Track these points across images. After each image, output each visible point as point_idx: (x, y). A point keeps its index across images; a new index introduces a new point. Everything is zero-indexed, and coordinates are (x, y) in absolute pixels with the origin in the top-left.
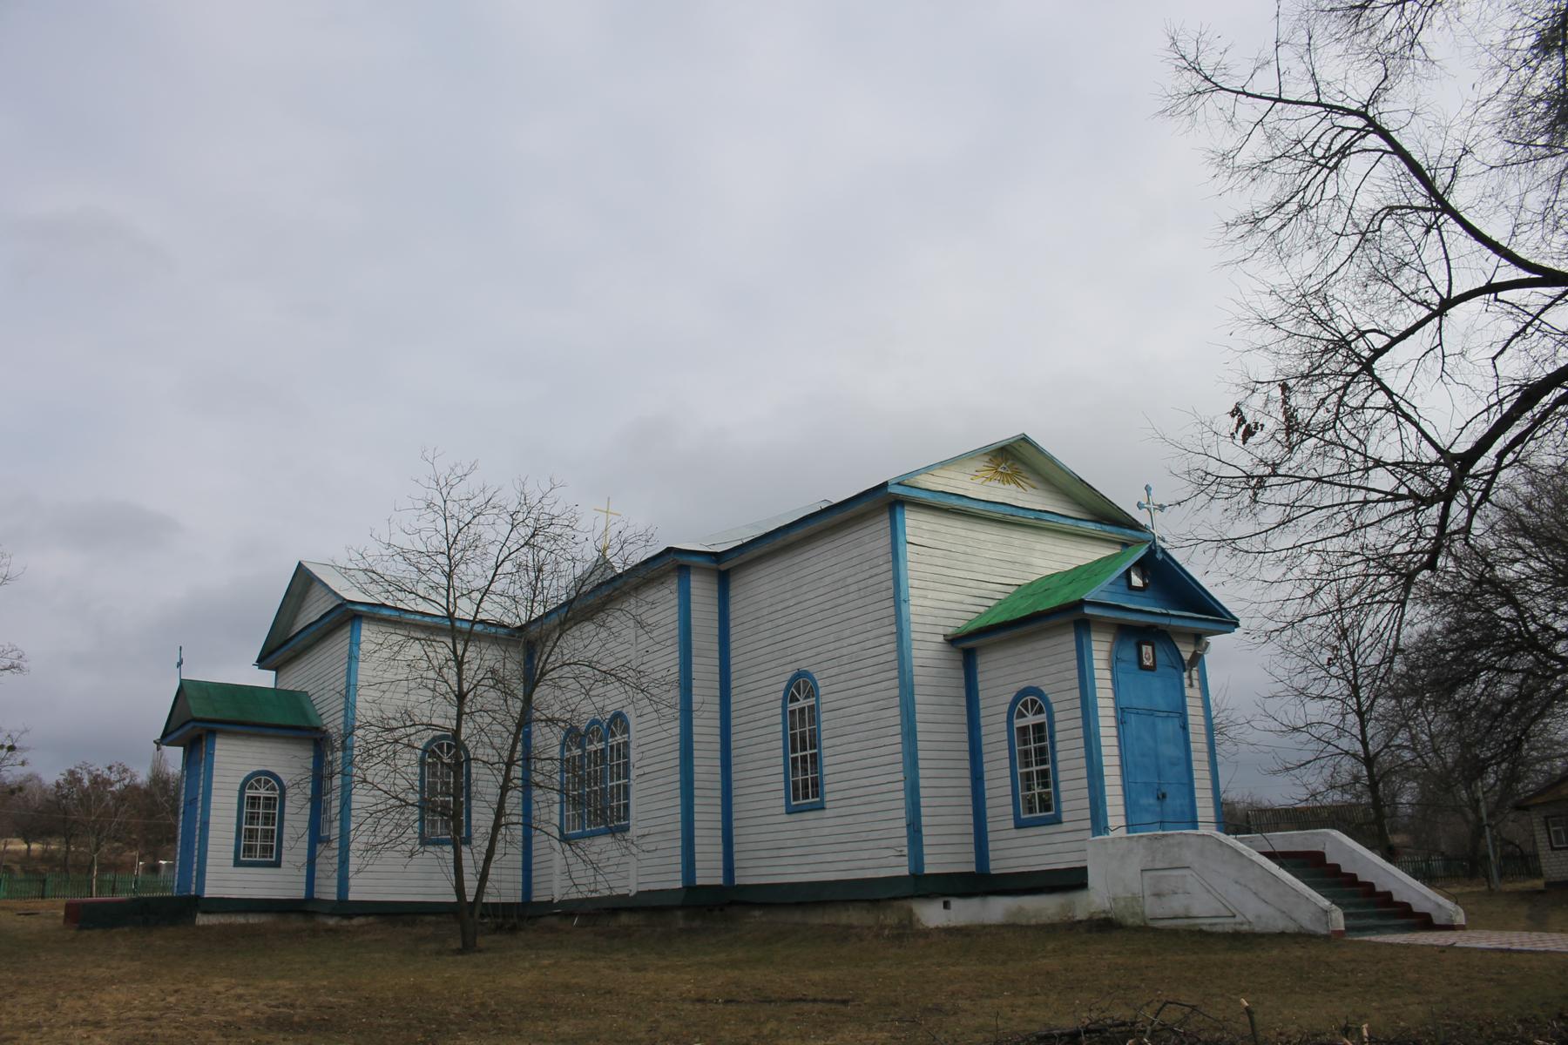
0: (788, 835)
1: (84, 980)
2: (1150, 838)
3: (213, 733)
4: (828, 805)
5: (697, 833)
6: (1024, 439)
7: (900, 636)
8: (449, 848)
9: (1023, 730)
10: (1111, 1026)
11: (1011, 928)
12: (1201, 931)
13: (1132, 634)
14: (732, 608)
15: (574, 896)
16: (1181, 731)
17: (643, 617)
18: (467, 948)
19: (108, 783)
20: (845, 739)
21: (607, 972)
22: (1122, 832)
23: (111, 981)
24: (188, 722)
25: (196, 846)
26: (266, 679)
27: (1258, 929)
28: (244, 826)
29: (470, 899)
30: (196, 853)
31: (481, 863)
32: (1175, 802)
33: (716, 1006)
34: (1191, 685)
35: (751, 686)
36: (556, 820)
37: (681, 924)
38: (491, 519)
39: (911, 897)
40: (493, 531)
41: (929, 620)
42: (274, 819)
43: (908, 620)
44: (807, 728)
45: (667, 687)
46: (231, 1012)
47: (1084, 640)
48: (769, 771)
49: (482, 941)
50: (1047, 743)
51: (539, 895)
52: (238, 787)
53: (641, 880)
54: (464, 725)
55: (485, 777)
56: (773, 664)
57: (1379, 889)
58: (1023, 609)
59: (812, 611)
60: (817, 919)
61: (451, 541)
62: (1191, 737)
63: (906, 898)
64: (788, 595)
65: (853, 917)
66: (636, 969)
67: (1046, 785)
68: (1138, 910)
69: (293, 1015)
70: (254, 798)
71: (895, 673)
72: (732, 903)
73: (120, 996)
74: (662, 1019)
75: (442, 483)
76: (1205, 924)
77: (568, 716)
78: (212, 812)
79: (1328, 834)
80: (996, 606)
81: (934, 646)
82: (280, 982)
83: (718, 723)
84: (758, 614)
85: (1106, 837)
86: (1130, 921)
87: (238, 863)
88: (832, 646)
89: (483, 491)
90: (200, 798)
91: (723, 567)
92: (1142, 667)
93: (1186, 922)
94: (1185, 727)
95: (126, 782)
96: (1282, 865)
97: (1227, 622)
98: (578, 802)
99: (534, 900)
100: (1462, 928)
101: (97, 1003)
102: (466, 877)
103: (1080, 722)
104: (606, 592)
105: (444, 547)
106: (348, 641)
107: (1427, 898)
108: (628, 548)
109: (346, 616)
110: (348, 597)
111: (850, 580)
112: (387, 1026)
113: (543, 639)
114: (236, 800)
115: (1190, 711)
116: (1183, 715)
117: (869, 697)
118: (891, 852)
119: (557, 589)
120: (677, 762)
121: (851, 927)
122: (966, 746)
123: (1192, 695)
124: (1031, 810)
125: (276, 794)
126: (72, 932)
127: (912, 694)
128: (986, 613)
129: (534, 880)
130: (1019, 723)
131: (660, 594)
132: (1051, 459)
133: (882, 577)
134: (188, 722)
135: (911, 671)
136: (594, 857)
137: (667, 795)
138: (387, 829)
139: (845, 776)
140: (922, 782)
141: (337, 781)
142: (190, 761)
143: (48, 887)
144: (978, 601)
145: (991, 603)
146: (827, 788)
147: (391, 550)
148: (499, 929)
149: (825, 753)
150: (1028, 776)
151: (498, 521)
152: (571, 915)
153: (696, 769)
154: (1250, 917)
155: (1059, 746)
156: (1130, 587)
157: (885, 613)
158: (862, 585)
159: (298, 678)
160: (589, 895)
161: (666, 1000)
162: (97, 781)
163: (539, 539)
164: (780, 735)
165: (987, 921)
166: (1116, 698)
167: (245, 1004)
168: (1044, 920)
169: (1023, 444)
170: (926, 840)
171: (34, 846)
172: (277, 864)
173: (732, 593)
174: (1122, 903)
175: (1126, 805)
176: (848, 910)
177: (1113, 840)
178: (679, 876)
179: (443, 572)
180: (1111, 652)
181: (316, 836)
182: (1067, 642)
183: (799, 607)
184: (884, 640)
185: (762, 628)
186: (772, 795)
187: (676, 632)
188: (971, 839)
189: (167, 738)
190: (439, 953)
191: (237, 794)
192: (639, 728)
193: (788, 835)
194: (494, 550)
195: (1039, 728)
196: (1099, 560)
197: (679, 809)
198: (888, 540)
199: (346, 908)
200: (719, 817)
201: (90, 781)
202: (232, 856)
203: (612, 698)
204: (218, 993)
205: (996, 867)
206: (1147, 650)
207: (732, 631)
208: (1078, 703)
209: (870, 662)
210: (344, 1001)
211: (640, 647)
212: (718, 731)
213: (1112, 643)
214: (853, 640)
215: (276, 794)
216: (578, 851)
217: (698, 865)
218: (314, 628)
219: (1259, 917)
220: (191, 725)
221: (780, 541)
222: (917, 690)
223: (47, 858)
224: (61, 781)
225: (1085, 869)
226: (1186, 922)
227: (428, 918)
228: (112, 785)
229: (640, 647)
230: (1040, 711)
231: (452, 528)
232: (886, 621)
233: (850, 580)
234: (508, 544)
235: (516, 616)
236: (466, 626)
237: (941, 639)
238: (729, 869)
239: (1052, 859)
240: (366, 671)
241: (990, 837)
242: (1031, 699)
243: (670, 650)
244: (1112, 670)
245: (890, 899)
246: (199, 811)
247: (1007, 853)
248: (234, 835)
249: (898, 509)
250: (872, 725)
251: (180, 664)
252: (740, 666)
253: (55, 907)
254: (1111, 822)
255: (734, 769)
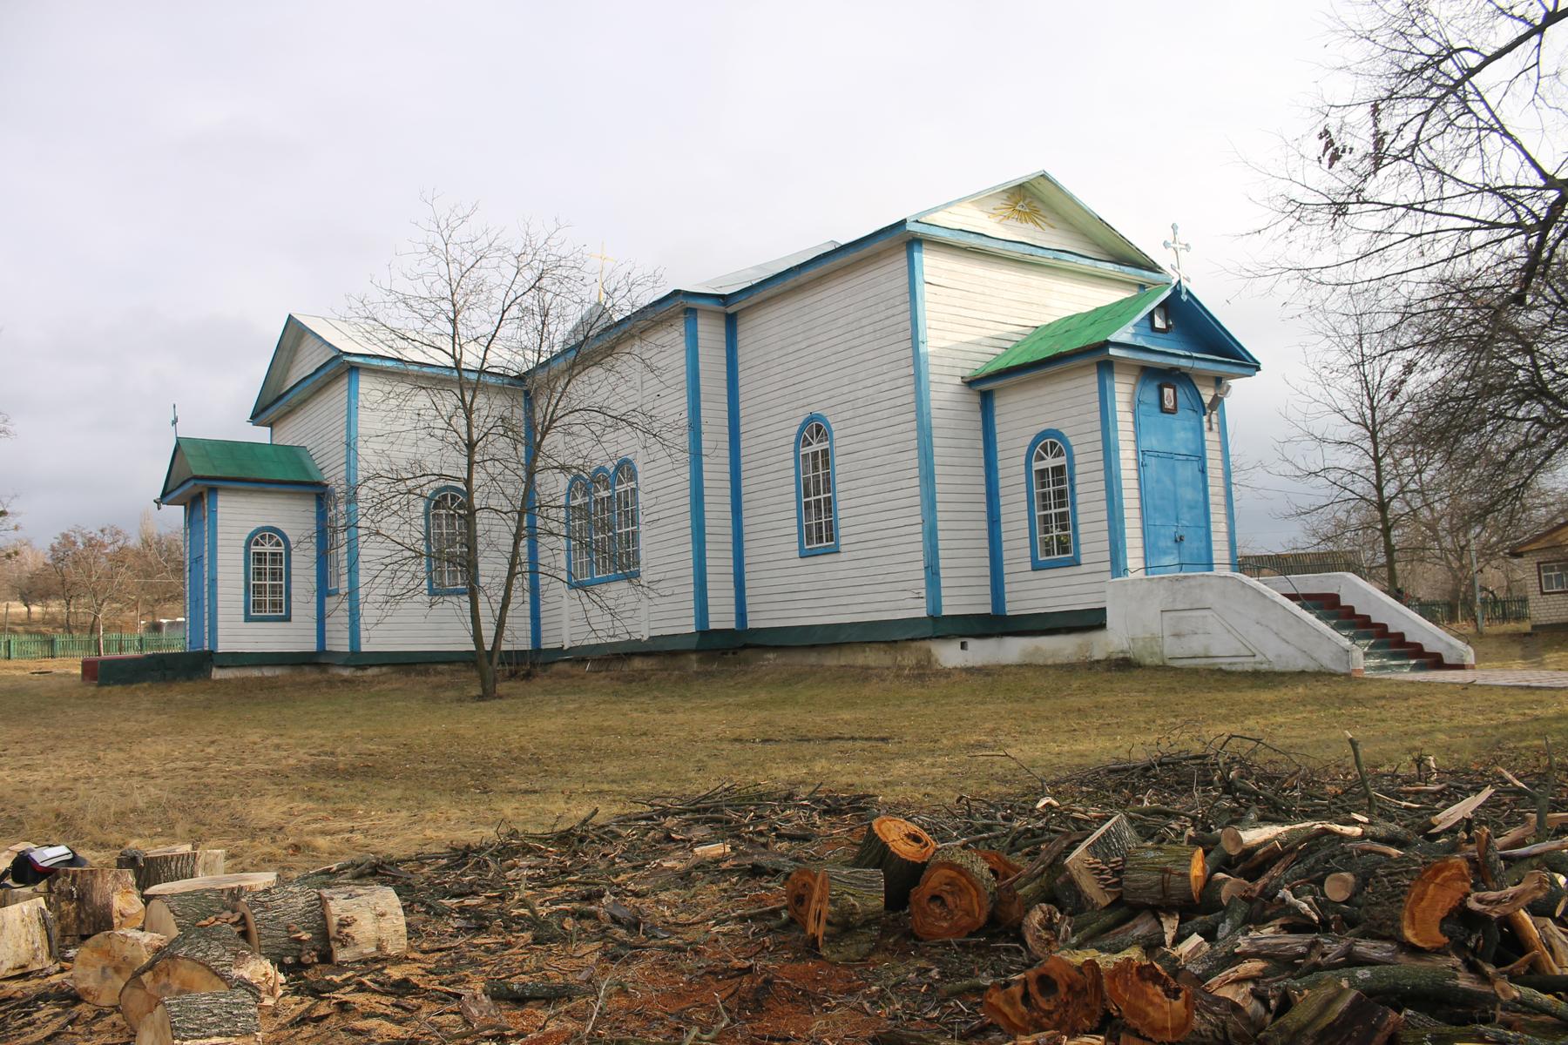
0: (801, 579)
1: (117, 733)
2: (1171, 580)
3: (214, 491)
4: (842, 549)
5: (709, 578)
6: (1044, 176)
7: (917, 377)
8: (466, 598)
9: (1042, 473)
10: (1185, 759)
11: (1025, 668)
12: (1220, 670)
13: (1159, 377)
14: (740, 352)
15: (593, 642)
16: (1199, 474)
17: (653, 360)
18: (487, 695)
19: (102, 545)
20: (859, 483)
21: (635, 715)
22: (1141, 574)
23: (144, 734)
24: (188, 480)
25: (206, 602)
26: (261, 435)
27: (1277, 668)
28: (252, 582)
29: (488, 648)
30: (206, 609)
31: (498, 613)
32: (1193, 545)
33: (754, 746)
34: (1211, 429)
35: (762, 431)
36: (564, 566)
37: (695, 667)
38: (495, 262)
39: (930, 638)
40: (499, 277)
41: (947, 362)
42: (281, 575)
43: (926, 362)
44: (821, 472)
45: (680, 431)
46: (277, 761)
47: (1107, 382)
48: (783, 516)
49: (502, 688)
50: (1067, 486)
51: (548, 642)
52: (243, 544)
53: (653, 625)
54: (475, 476)
55: (497, 528)
56: (785, 408)
57: (1391, 630)
58: (1045, 351)
59: (824, 353)
60: (832, 660)
61: (454, 287)
62: (1209, 480)
63: (924, 639)
64: (799, 338)
65: (870, 658)
66: (663, 711)
67: (1064, 528)
68: (1157, 649)
69: (337, 763)
70: (259, 554)
71: (912, 416)
72: (746, 647)
73: (159, 748)
74: (705, 759)
75: (443, 226)
76: (1224, 663)
77: (581, 461)
78: (219, 569)
79: (1344, 577)
80: (1013, 348)
81: (952, 389)
82: (314, 732)
83: (728, 468)
84: (768, 358)
85: (1125, 578)
86: (1148, 661)
87: (248, 618)
88: (846, 389)
89: (486, 232)
90: (206, 555)
91: (730, 310)
92: (1163, 409)
93: (1204, 661)
94: (1203, 471)
95: (120, 544)
96: (1303, 606)
97: (1249, 364)
98: (587, 547)
99: (543, 647)
100: (1472, 667)
101: (138, 755)
102: (483, 626)
103: (1101, 465)
104: (613, 335)
105: (447, 293)
106: (346, 393)
107: (1439, 639)
108: (636, 290)
109: (343, 368)
110: (346, 347)
111: (864, 322)
112: (432, 772)
113: (550, 385)
114: (242, 557)
115: (1209, 454)
116: (1201, 458)
117: (885, 441)
118: (910, 595)
119: (560, 333)
120: (688, 508)
121: (868, 668)
122: (983, 489)
123: (1211, 438)
124: (1048, 553)
125: (282, 549)
126: (92, 688)
127: (930, 436)
128: (1004, 355)
129: (543, 628)
130: (1037, 466)
131: (668, 338)
132: (1071, 198)
133: (900, 318)
134: (188, 480)
135: (929, 413)
136: (611, 603)
137: (678, 541)
138: (403, 581)
139: (861, 519)
140: (940, 525)
141: (342, 537)
142: (192, 520)
143: (58, 647)
144: (996, 343)
145: (1009, 345)
146: (841, 532)
147: (392, 297)
148: (513, 675)
149: (839, 496)
150: (1046, 519)
151: (503, 264)
152: (584, 660)
153: (707, 515)
154: (1271, 656)
155: (1078, 489)
156: (1153, 328)
157: (903, 354)
158: (878, 326)
159: (293, 433)
160: (609, 640)
161: (703, 740)
162: (90, 543)
163: (544, 282)
164: (793, 480)
165: (1004, 662)
166: (1137, 441)
167: (285, 753)
168: (1060, 660)
169: (1042, 181)
170: (943, 583)
171: (34, 609)
172: (287, 619)
173: (739, 337)
174: (1141, 643)
175: (1144, 547)
176: (864, 651)
177: (1133, 582)
178: (693, 621)
179: (448, 317)
180: (1133, 394)
181: (324, 590)
182: (1090, 382)
183: (812, 349)
184: (901, 382)
185: (772, 372)
186: (785, 539)
187: (684, 377)
188: (988, 581)
189: (166, 496)
190: (459, 700)
191: (242, 550)
192: (648, 474)
193: (801, 579)
194: (499, 294)
195: (1059, 470)
196: (1121, 302)
197: (690, 555)
198: (905, 279)
199: (359, 660)
200: (731, 562)
201: (84, 544)
202: (242, 611)
203: (625, 443)
204: (255, 743)
205: (1012, 608)
206: (1168, 392)
207: (741, 375)
208: (1100, 445)
209: (888, 404)
210: (383, 748)
211: (645, 393)
212: (728, 476)
213: (1134, 385)
214: (869, 383)
215: (282, 549)
216: (594, 597)
217: (711, 610)
218: (309, 381)
219: (1279, 656)
220: (192, 483)
221: (791, 282)
222: (935, 433)
223: (50, 621)
224: (56, 545)
225: (1104, 609)
226: (1204, 661)
227: (440, 667)
228: (106, 547)
229: (645, 393)
230: (1060, 454)
231: (455, 275)
232: (903, 363)
233: (864, 322)
234: (514, 287)
235: (520, 362)
236: (473, 377)
237: (959, 381)
238: (741, 614)
239: (1070, 600)
240: (367, 422)
241: (1007, 579)
242: (1050, 441)
243: (678, 395)
244: (1134, 412)
245: (907, 640)
246: (206, 568)
247: (1024, 595)
248: (242, 591)
249: (916, 247)
250: (888, 468)
251: (175, 422)
252: (750, 411)
253: (73, 666)
254: (1131, 564)
255: (745, 514)
